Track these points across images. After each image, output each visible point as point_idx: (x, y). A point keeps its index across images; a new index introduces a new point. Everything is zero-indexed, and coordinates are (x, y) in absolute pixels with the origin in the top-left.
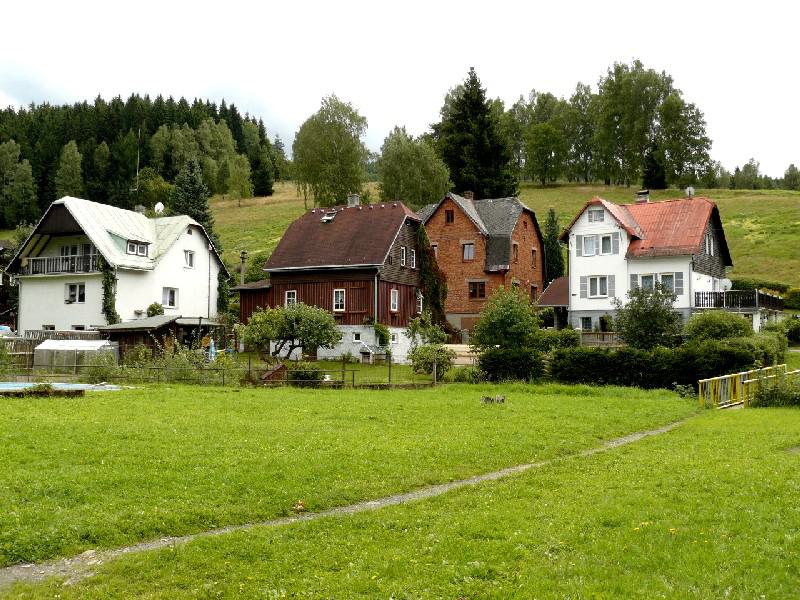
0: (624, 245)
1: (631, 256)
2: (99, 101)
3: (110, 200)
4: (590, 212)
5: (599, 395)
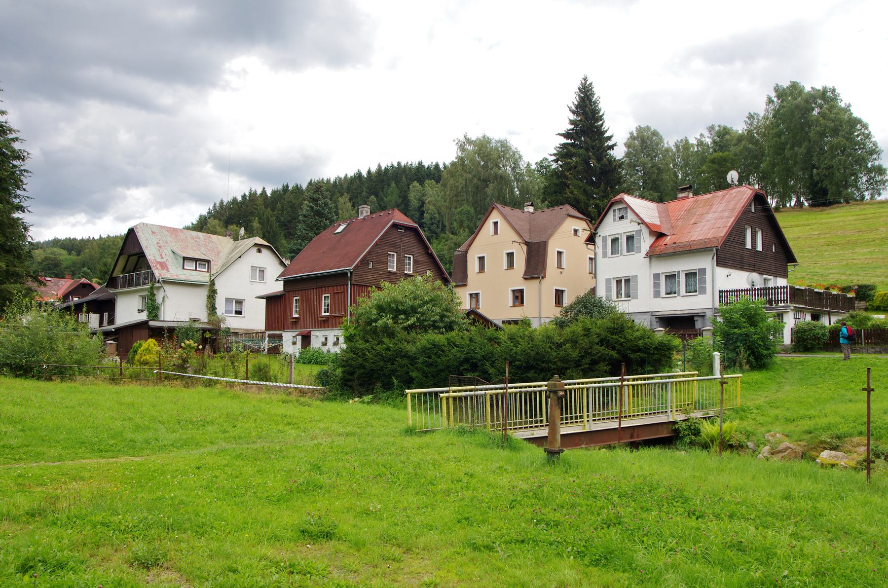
0: (646, 242)
1: (653, 255)
2: (420, 164)
3: (137, 250)
4: (614, 211)
5: (309, 406)
